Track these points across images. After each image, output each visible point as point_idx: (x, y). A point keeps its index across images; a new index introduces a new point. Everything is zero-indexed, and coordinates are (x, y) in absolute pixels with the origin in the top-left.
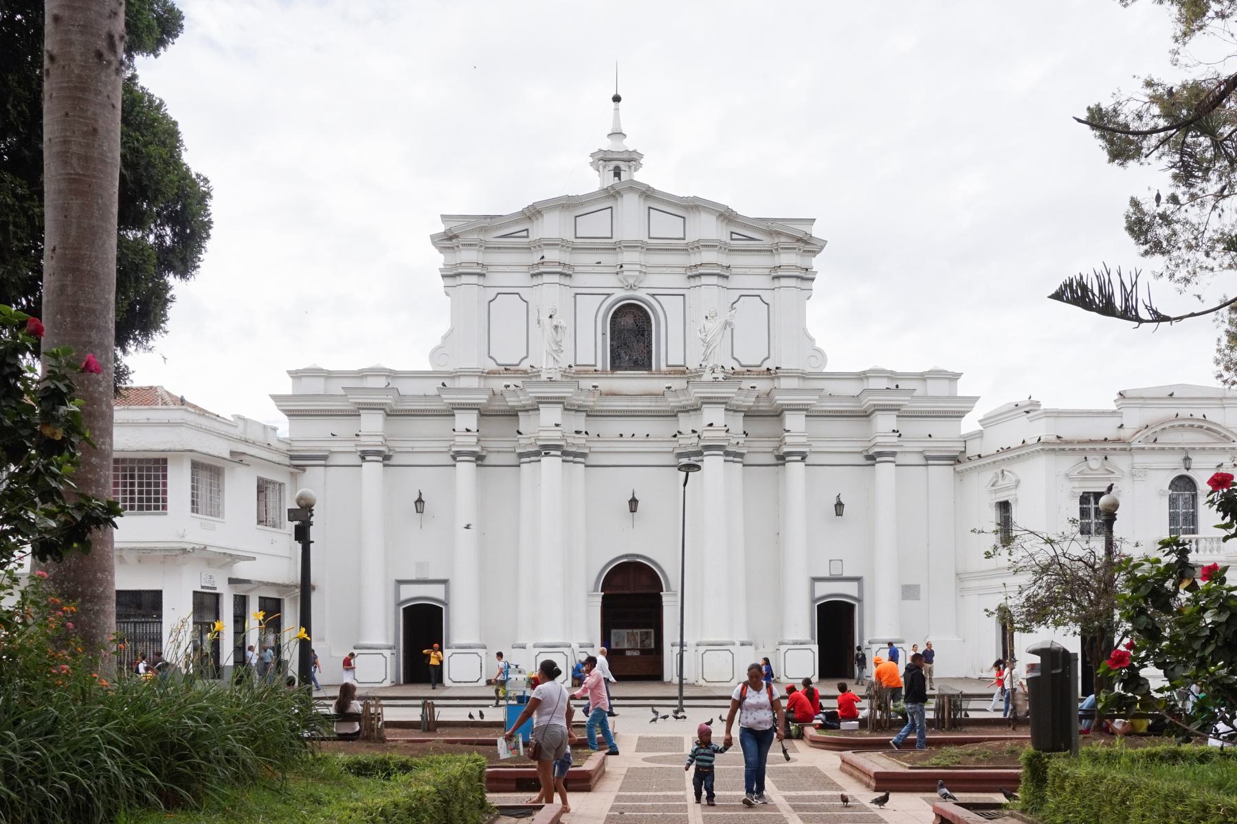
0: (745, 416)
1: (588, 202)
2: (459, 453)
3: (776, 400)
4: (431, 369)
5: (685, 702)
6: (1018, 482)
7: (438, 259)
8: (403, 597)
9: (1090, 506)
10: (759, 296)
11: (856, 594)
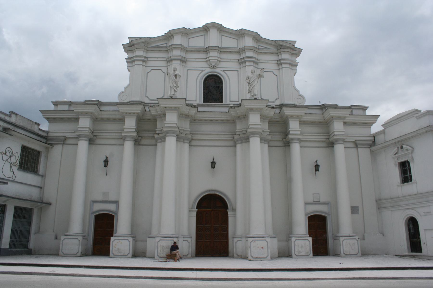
1: (202, 120)
4: (118, 101)
7: (126, 56)
9: (408, 175)
10: (272, 72)
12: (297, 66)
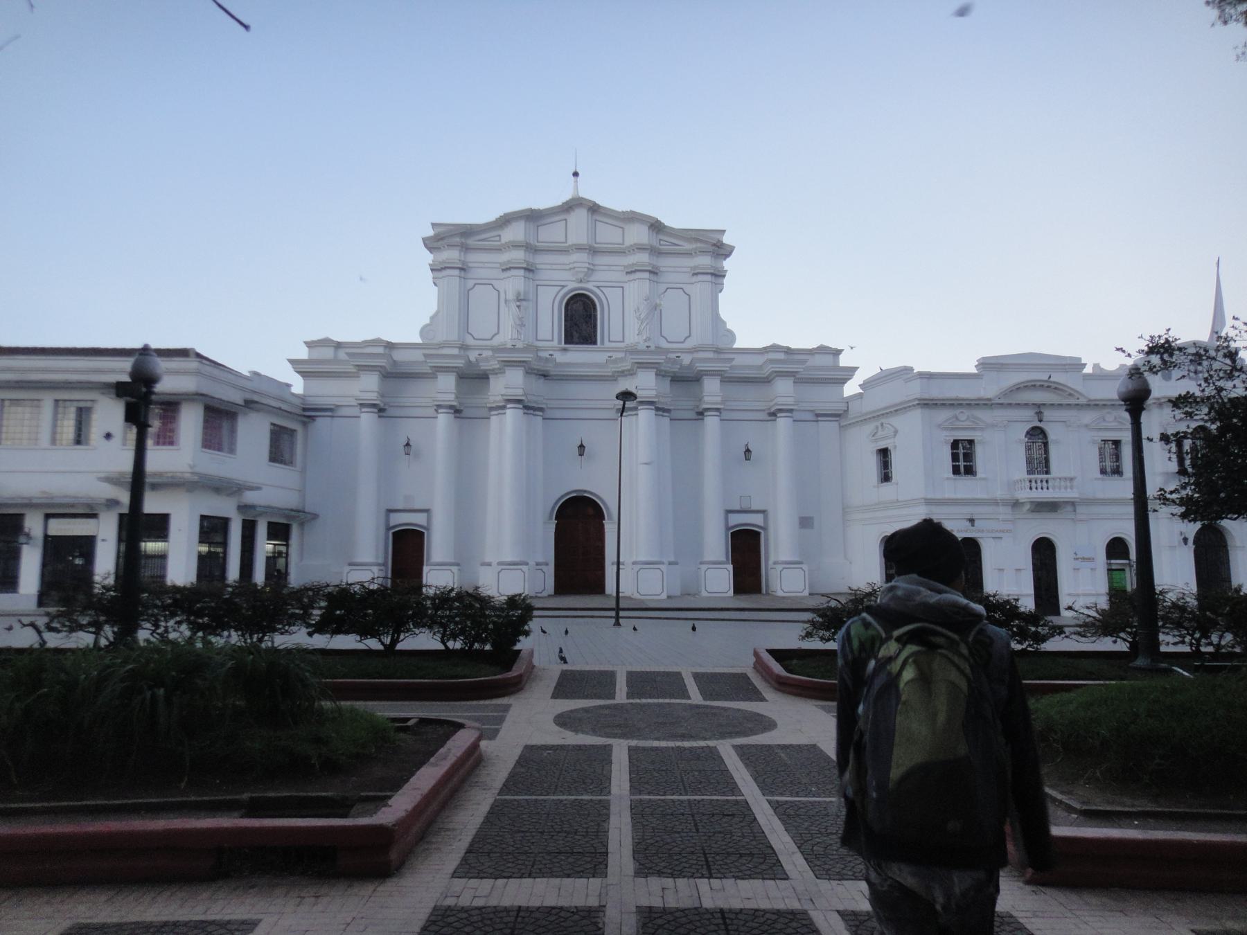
0: (671, 381)
2: (439, 406)
3: (697, 367)
4: (421, 342)
5: (622, 614)
6: (896, 432)
7: (429, 257)
8: (731, 523)
11: (762, 524)
12: (724, 276)
